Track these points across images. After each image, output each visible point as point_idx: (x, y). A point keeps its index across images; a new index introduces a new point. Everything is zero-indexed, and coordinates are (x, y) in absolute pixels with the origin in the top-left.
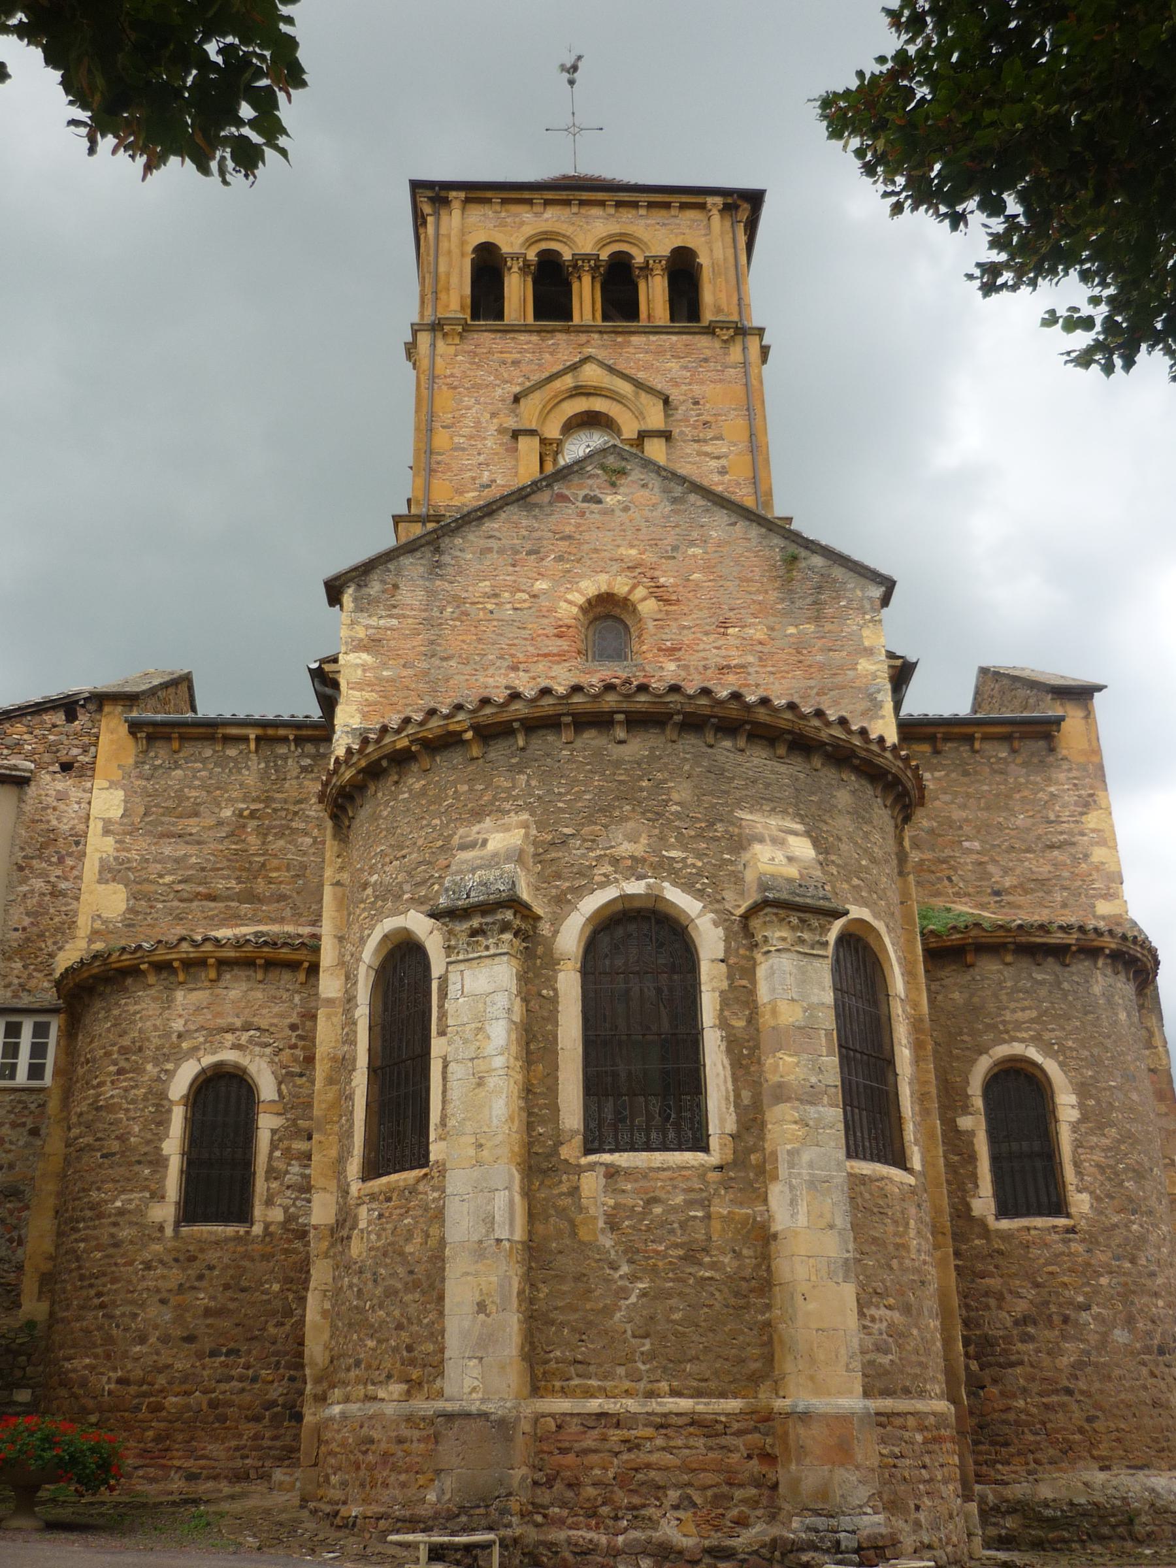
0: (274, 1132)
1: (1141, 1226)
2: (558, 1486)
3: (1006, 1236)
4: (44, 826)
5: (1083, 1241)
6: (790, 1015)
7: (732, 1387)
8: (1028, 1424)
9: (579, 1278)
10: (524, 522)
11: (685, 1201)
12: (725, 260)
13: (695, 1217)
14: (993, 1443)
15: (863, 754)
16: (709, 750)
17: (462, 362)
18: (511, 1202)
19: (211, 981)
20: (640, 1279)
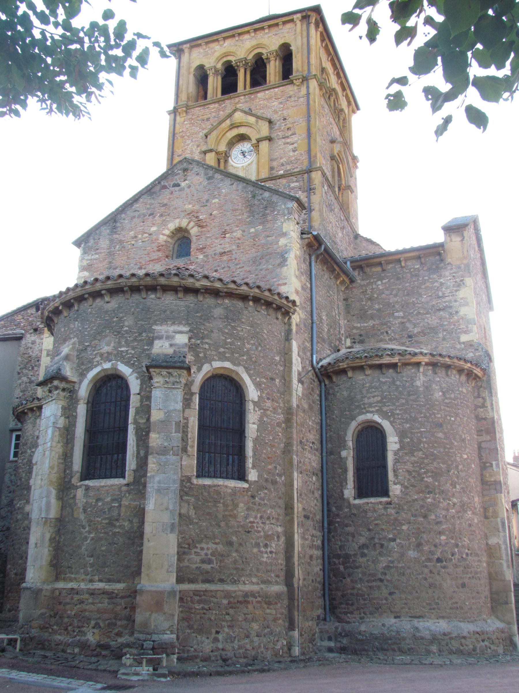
3: (358, 507)
5: (394, 508)
10: (149, 202)
11: (111, 500)
12: (302, 45)
13: (114, 506)
15: (225, 290)
16: (144, 300)
17: (187, 124)
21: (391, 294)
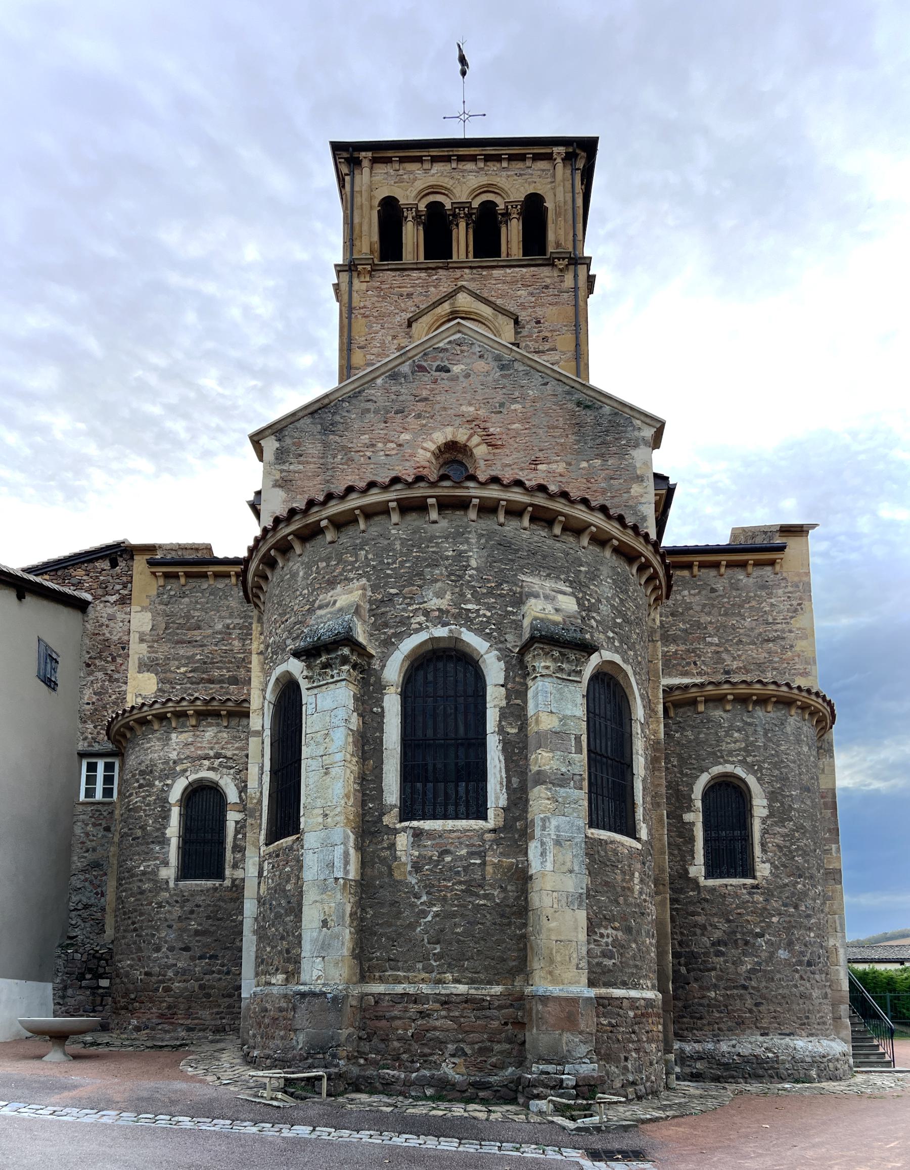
0: (237, 822)
1: (805, 886)
2: (375, 1040)
3: (713, 890)
4: (101, 638)
6: (548, 723)
7: (496, 977)
8: (715, 1006)
9: (394, 903)
10: (394, 389)
11: (467, 853)
12: (565, 202)
13: (475, 864)
14: (692, 1017)
18: (346, 854)
19: (193, 726)
20: (435, 905)
21: (702, 611)
